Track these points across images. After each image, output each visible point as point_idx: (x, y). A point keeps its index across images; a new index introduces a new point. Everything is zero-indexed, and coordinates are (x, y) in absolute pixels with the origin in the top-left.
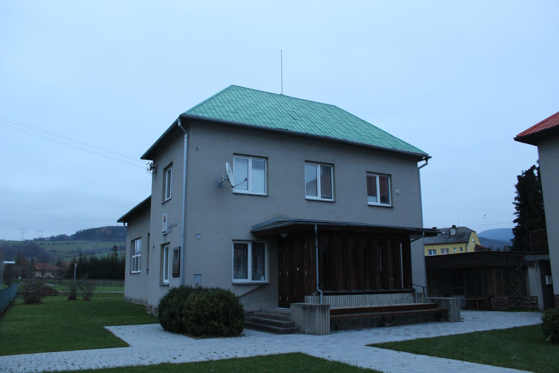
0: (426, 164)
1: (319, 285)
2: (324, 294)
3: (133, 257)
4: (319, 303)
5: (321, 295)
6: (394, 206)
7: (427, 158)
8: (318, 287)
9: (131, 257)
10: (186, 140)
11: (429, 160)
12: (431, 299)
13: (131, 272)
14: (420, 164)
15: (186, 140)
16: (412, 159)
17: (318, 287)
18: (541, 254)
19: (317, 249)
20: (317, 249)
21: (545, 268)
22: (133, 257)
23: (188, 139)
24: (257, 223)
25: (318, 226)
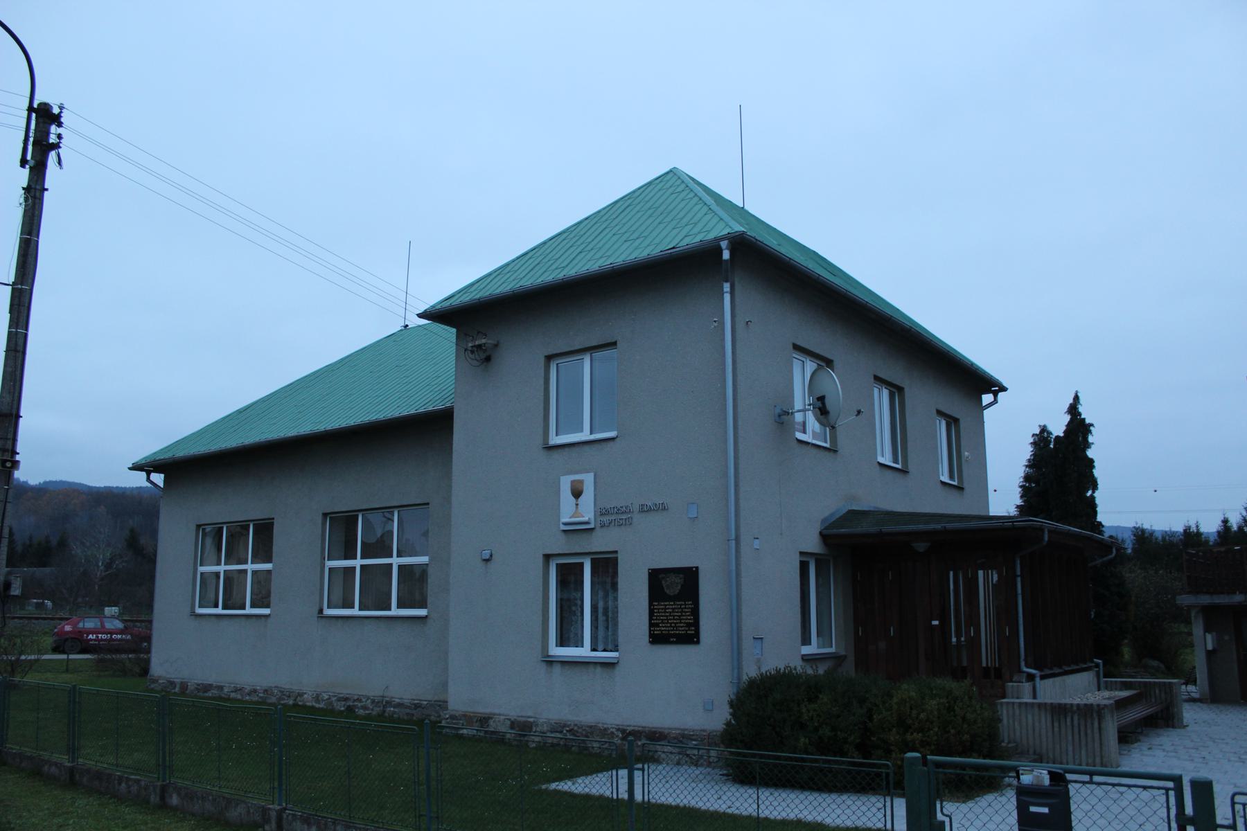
0: (995, 401)
1: (1026, 660)
2: (1042, 678)
3: (201, 569)
4: (1035, 697)
5: (1038, 679)
6: (966, 485)
7: (1003, 389)
8: (1023, 664)
9: (195, 570)
10: (727, 297)
11: (1000, 394)
12: (1122, 682)
13: (321, 611)
14: (987, 398)
15: (727, 297)
16: (992, 386)
17: (1023, 664)
18: (1211, 594)
19: (1019, 579)
20: (1019, 579)
21: (616, 599)
22: (201, 569)
23: (732, 293)
24: (827, 514)
25: (1050, 532)
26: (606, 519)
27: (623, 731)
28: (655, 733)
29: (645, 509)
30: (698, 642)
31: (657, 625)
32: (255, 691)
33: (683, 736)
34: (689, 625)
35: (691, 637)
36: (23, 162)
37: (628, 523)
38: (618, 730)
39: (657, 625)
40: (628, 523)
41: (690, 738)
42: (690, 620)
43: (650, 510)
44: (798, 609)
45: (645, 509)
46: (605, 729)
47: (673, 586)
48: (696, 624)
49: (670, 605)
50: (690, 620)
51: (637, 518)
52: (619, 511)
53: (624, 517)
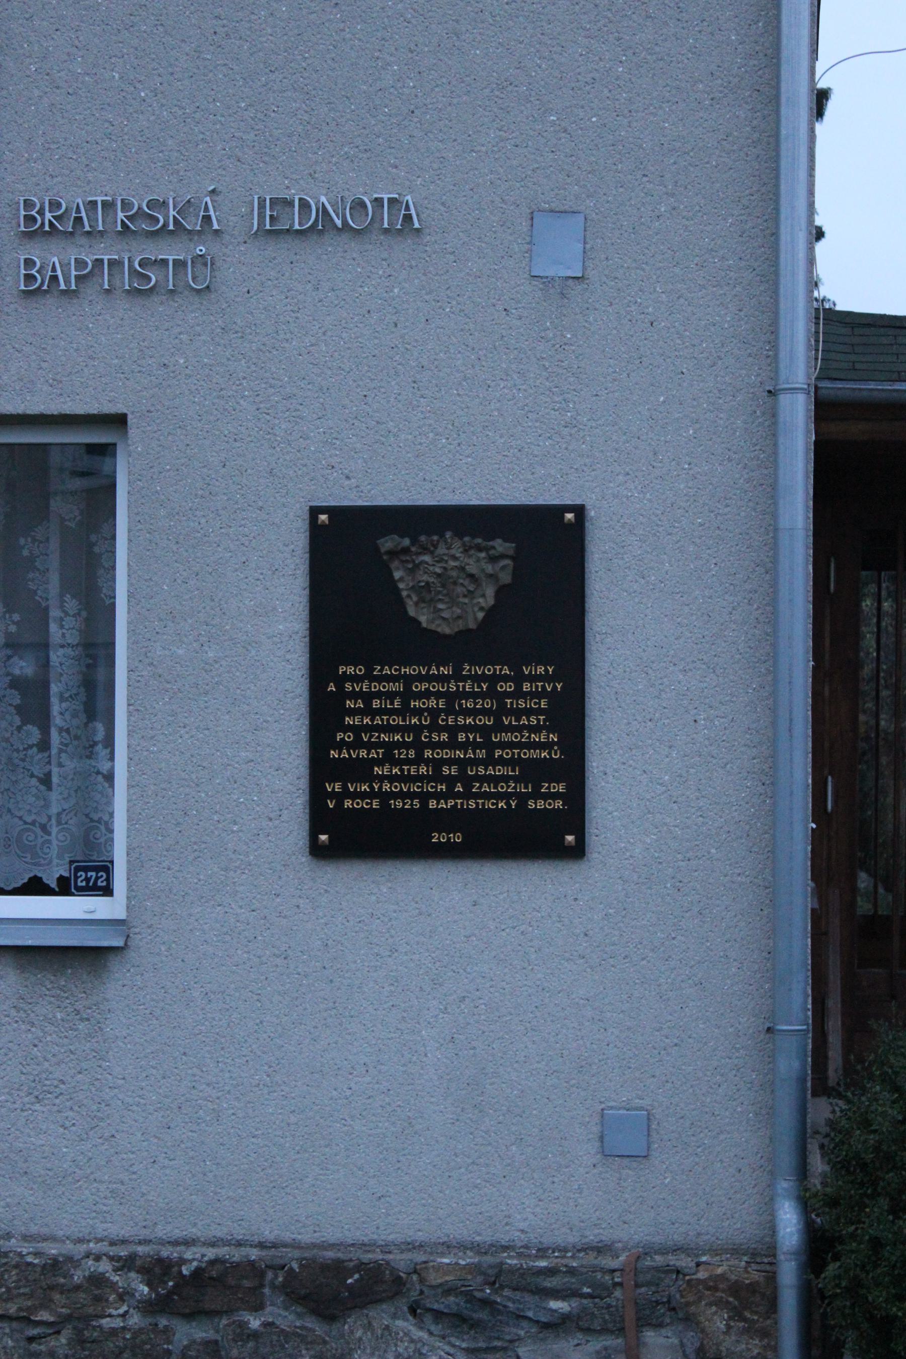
17: (152, 284)
26: (56, 257)
27: (157, 1269)
28: (338, 1268)
29: (289, 226)
30: (578, 852)
31: (362, 770)
32: (542, 1340)
33: (497, 1277)
34: (534, 772)
35: (542, 823)
36: (822, 97)
37: (195, 283)
38: (126, 1264)
39: (362, 770)
40: (195, 283)
41: (532, 1283)
42: (545, 746)
43: (322, 227)
44: (93, 408)
45: (289, 226)
46: (55, 1265)
47: (454, 594)
48: (572, 768)
49: (432, 681)
50: (545, 746)
51: (240, 263)
52: (144, 223)
53: (171, 252)
